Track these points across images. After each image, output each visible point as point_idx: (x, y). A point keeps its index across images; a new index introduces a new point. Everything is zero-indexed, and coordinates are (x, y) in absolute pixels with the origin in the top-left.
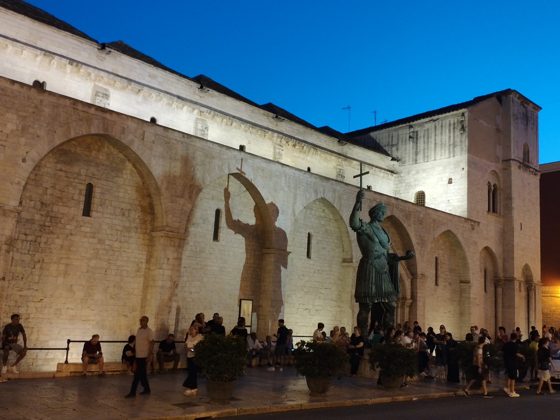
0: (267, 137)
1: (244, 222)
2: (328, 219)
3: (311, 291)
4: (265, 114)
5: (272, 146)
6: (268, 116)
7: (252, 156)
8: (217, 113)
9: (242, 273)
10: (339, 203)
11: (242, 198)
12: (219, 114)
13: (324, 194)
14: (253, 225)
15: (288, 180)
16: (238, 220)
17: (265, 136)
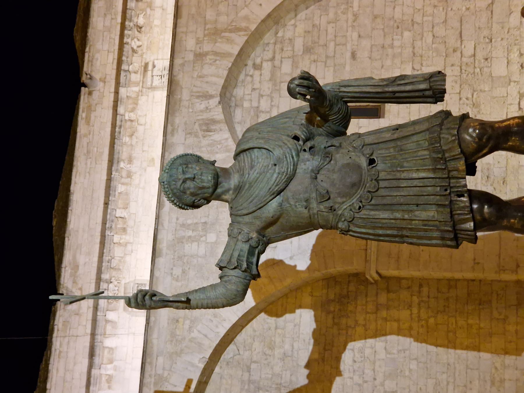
0: (132, 114)
1: (311, 348)
2: (278, 46)
3: (470, 96)
4: (86, 117)
5: (151, 94)
6: (90, 109)
7: (148, 360)
8: (104, 264)
9: (437, 346)
10: (227, 34)
11: (255, 358)
12: (106, 258)
13: (211, 97)
14: (315, 316)
15: (190, 233)
16: (307, 366)
17: (132, 121)
